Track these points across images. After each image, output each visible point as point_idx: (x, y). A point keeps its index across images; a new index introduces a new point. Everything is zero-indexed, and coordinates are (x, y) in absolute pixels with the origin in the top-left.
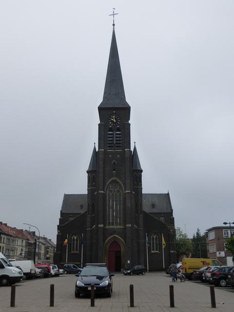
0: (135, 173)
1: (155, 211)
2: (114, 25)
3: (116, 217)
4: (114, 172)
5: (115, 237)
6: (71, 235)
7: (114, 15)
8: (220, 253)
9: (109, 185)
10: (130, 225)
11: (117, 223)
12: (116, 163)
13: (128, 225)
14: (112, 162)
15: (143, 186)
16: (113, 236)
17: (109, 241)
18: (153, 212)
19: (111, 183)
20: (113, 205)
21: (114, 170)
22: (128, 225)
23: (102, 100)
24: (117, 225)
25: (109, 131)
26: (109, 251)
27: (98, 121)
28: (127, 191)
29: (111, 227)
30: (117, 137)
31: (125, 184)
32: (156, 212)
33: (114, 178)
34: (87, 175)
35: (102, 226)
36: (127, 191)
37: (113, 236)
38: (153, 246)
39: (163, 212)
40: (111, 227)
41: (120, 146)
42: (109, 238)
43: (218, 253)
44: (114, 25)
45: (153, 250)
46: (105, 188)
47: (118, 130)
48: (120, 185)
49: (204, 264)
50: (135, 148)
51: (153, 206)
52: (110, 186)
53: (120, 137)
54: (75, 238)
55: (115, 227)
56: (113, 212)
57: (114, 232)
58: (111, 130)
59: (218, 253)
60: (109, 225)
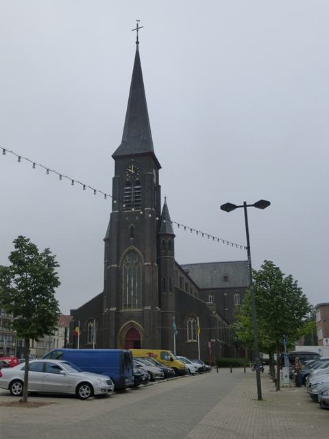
0: (169, 239)
1: (227, 285)
2: (137, 43)
3: (134, 296)
4: (132, 239)
5: (132, 323)
6: (87, 321)
7: (137, 29)
8: (327, 341)
9: (124, 257)
10: (149, 308)
11: (134, 305)
12: (134, 226)
13: (146, 308)
14: (130, 227)
15: (175, 254)
16: (129, 322)
17: (126, 326)
18: (224, 287)
19: (128, 253)
20: (130, 282)
21: (132, 237)
22: (146, 308)
23: (119, 143)
24: (134, 307)
25: (127, 186)
26: (126, 341)
27: (111, 173)
28: (146, 264)
29: (127, 310)
30: (135, 193)
31: (144, 255)
32: (228, 286)
33: (132, 247)
34: (104, 242)
35: (114, 309)
36: (146, 264)
37: (129, 322)
38: (190, 334)
39: (238, 286)
40: (127, 310)
41: (139, 205)
42: (124, 326)
43: (325, 340)
44: (137, 43)
45: (190, 339)
46: (120, 261)
47: (138, 183)
48: (140, 257)
49: (150, 356)
50: (165, 206)
51: (226, 279)
52: (127, 257)
53: (139, 193)
54: (192, 322)
55: (132, 310)
56: (130, 290)
57: (131, 316)
58: (128, 184)
59: (325, 340)
60: (125, 308)
